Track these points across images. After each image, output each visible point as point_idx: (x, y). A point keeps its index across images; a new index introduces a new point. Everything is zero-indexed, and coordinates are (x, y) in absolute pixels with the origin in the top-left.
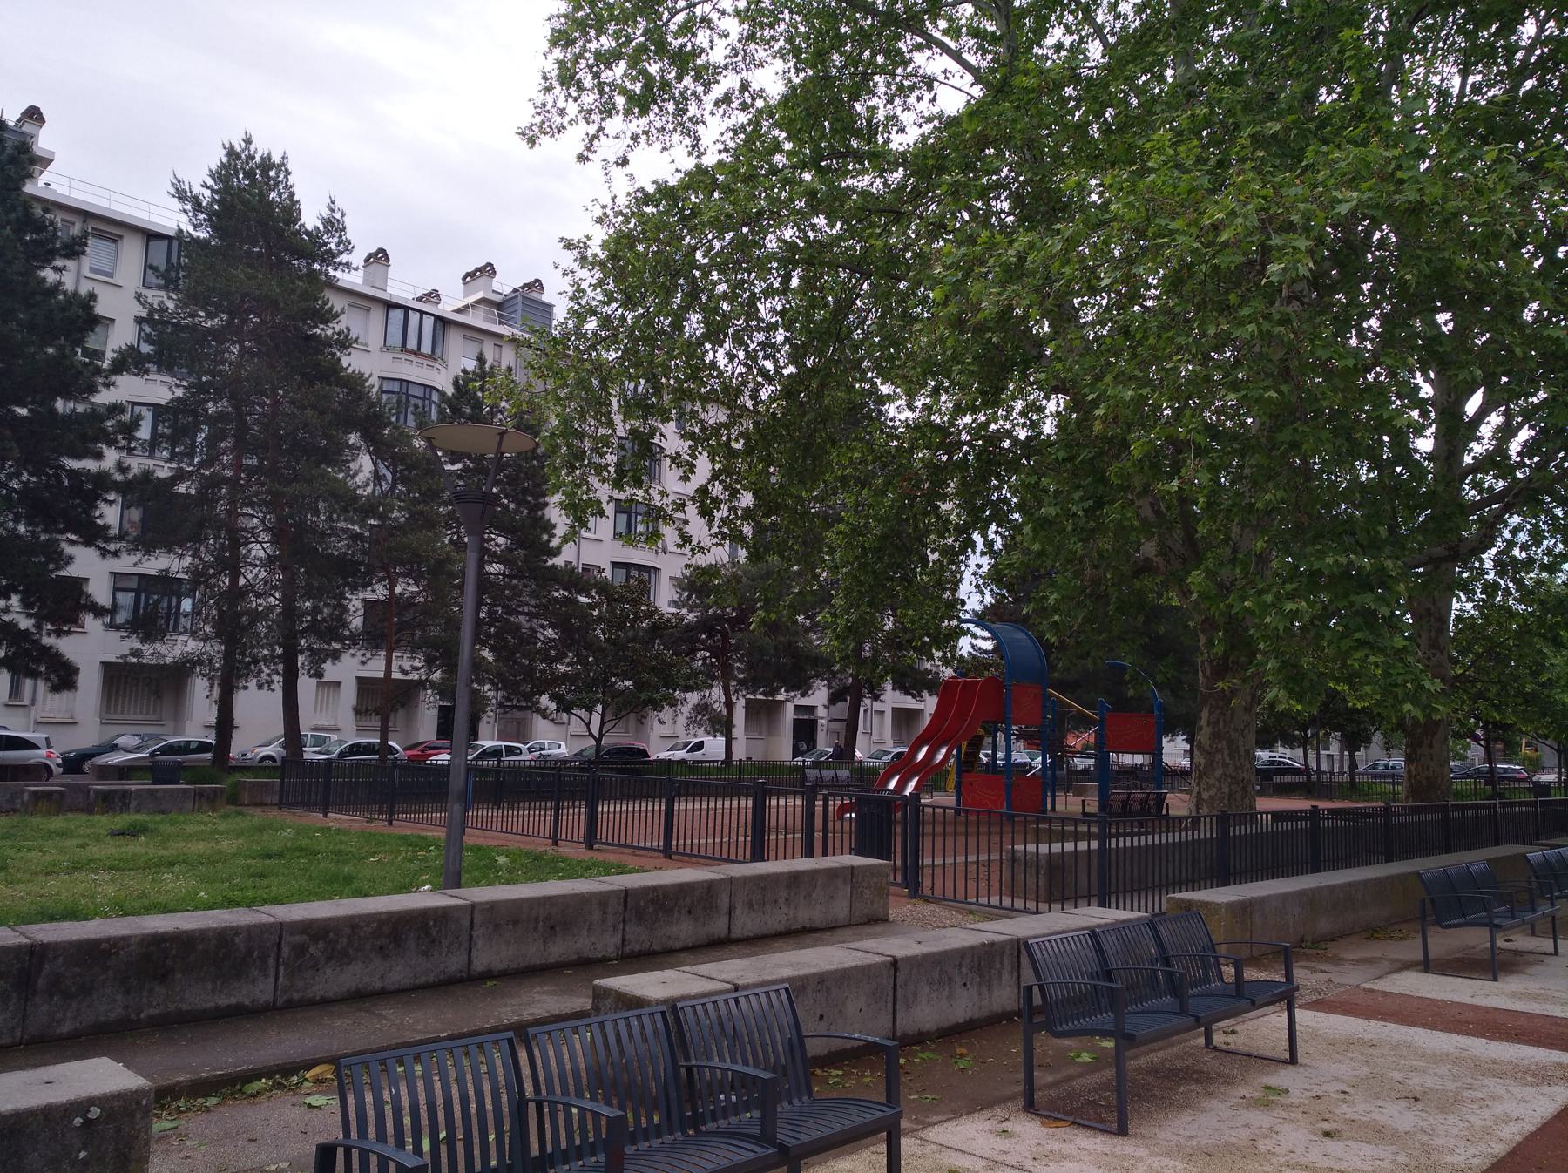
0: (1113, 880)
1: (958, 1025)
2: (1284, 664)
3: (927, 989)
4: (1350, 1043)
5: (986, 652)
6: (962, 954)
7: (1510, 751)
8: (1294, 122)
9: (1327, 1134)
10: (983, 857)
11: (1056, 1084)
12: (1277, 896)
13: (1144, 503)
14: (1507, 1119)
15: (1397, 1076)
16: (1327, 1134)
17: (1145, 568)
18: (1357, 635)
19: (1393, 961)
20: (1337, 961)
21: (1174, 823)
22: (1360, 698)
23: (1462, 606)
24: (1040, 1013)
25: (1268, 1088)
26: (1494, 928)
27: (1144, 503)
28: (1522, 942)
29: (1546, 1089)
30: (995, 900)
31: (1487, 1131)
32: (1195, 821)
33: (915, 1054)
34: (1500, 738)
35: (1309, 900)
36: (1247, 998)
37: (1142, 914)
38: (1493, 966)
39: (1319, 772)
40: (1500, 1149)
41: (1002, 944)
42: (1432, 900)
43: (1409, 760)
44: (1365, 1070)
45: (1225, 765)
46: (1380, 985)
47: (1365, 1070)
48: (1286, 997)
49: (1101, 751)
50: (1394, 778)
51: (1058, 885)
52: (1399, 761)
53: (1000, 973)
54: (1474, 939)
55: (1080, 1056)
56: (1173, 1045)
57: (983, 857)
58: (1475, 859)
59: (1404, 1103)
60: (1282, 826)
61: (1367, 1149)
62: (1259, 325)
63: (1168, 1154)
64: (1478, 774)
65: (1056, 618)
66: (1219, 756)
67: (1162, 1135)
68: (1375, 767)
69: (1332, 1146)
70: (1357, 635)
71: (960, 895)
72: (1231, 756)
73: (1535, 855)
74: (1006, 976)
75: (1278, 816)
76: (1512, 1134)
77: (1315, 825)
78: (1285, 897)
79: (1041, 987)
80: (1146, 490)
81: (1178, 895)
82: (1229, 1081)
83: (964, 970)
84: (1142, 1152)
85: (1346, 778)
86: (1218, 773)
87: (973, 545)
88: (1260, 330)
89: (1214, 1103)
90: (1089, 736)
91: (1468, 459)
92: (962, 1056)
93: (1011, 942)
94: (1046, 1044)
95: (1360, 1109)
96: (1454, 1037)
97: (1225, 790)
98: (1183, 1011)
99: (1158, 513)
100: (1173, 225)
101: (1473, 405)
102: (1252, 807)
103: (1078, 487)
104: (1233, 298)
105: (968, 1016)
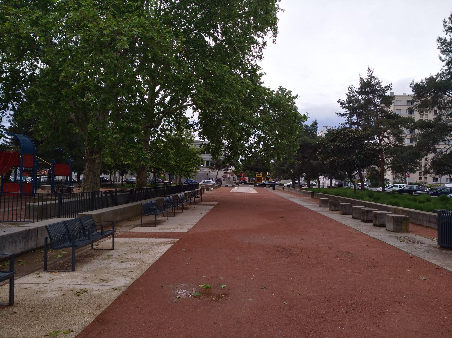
0: (62, 211)
1: (18, 254)
2: (111, 151)
3: (8, 245)
4: (126, 243)
5: (8, 143)
6: (19, 233)
7: (159, 176)
8: (121, 3)
9: (122, 262)
10: (15, 208)
11: (52, 264)
12: (107, 212)
13: (72, 102)
14: (158, 253)
15: (136, 248)
16: (122, 262)
17: (71, 121)
18: (131, 144)
19: (134, 225)
20: (121, 226)
21: (76, 195)
22: (126, 161)
23: (152, 139)
24: (51, 245)
25: (108, 255)
26: (156, 215)
27: (72, 102)
28: (161, 218)
29: (166, 246)
30: (23, 220)
31: (155, 256)
32: (83, 194)
33: (4, 264)
34: (157, 172)
35: (115, 212)
36: (104, 236)
37: (72, 218)
38: (155, 223)
39: (114, 181)
40: (157, 258)
41: (32, 230)
42: (144, 210)
43: (138, 177)
44: (129, 248)
45: (92, 179)
46: (131, 231)
47: (129, 248)
48: (113, 235)
49: (51, 175)
50: (133, 182)
51: (43, 214)
52: (135, 179)
53: (31, 238)
54: (151, 218)
55: (57, 255)
56: (83, 250)
57: (15, 208)
58: (153, 200)
59: (138, 253)
60: (106, 195)
61: (131, 263)
62: (111, 60)
63: (86, 273)
64: (152, 181)
65: (41, 133)
66: (90, 176)
67: (83, 269)
68: (127, 180)
69: (123, 264)
70: (131, 144)
71: (10, 219)
72: (94, 176)
73: (165, 198)
74: (33, 238)
75: (105, 192)
76: (159, 255)
77: (116, 194)
78: (109, 212)
79: (50, 238)
80: (73, 98)
81: (82, 213)
82: (98, 255)
83: (20, 238)
84: (79, 274)
85: (120, 183)
86: (90, 181)
87: (8, 107)
88: (111, 61)
89: (95, 260)
90: (46, 172)
91: (156, 101)
92: (20, 262)
93: (35, 229)
94: (51, 253)
95: (129, 256)
96: (148, 239)
97: (92, 185)
98: (89, 239)
99: (76, 106)
100: (89, 25)
101: (157, 88)
102: (99, 190)
103: (52, 94)
104: (104, 50)
105: (21, 251)
